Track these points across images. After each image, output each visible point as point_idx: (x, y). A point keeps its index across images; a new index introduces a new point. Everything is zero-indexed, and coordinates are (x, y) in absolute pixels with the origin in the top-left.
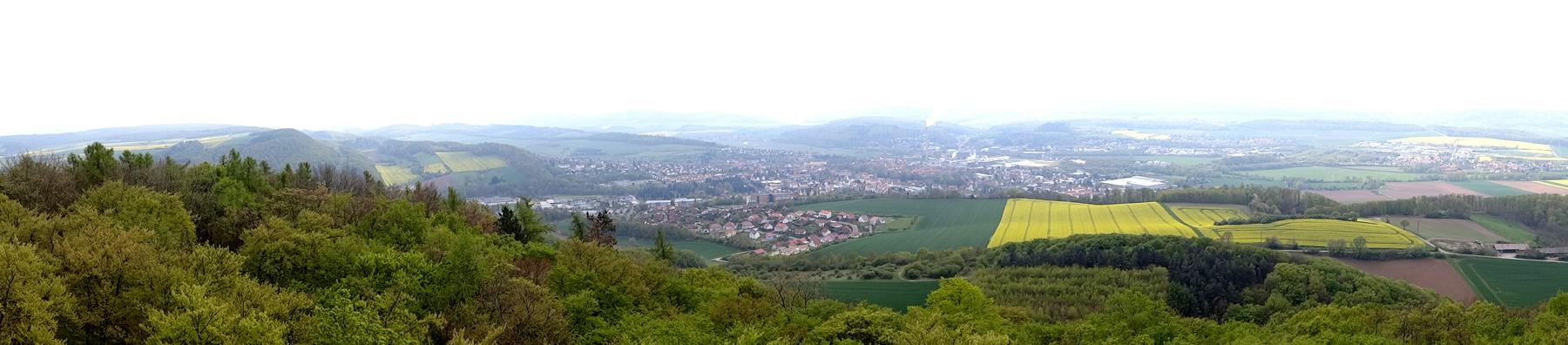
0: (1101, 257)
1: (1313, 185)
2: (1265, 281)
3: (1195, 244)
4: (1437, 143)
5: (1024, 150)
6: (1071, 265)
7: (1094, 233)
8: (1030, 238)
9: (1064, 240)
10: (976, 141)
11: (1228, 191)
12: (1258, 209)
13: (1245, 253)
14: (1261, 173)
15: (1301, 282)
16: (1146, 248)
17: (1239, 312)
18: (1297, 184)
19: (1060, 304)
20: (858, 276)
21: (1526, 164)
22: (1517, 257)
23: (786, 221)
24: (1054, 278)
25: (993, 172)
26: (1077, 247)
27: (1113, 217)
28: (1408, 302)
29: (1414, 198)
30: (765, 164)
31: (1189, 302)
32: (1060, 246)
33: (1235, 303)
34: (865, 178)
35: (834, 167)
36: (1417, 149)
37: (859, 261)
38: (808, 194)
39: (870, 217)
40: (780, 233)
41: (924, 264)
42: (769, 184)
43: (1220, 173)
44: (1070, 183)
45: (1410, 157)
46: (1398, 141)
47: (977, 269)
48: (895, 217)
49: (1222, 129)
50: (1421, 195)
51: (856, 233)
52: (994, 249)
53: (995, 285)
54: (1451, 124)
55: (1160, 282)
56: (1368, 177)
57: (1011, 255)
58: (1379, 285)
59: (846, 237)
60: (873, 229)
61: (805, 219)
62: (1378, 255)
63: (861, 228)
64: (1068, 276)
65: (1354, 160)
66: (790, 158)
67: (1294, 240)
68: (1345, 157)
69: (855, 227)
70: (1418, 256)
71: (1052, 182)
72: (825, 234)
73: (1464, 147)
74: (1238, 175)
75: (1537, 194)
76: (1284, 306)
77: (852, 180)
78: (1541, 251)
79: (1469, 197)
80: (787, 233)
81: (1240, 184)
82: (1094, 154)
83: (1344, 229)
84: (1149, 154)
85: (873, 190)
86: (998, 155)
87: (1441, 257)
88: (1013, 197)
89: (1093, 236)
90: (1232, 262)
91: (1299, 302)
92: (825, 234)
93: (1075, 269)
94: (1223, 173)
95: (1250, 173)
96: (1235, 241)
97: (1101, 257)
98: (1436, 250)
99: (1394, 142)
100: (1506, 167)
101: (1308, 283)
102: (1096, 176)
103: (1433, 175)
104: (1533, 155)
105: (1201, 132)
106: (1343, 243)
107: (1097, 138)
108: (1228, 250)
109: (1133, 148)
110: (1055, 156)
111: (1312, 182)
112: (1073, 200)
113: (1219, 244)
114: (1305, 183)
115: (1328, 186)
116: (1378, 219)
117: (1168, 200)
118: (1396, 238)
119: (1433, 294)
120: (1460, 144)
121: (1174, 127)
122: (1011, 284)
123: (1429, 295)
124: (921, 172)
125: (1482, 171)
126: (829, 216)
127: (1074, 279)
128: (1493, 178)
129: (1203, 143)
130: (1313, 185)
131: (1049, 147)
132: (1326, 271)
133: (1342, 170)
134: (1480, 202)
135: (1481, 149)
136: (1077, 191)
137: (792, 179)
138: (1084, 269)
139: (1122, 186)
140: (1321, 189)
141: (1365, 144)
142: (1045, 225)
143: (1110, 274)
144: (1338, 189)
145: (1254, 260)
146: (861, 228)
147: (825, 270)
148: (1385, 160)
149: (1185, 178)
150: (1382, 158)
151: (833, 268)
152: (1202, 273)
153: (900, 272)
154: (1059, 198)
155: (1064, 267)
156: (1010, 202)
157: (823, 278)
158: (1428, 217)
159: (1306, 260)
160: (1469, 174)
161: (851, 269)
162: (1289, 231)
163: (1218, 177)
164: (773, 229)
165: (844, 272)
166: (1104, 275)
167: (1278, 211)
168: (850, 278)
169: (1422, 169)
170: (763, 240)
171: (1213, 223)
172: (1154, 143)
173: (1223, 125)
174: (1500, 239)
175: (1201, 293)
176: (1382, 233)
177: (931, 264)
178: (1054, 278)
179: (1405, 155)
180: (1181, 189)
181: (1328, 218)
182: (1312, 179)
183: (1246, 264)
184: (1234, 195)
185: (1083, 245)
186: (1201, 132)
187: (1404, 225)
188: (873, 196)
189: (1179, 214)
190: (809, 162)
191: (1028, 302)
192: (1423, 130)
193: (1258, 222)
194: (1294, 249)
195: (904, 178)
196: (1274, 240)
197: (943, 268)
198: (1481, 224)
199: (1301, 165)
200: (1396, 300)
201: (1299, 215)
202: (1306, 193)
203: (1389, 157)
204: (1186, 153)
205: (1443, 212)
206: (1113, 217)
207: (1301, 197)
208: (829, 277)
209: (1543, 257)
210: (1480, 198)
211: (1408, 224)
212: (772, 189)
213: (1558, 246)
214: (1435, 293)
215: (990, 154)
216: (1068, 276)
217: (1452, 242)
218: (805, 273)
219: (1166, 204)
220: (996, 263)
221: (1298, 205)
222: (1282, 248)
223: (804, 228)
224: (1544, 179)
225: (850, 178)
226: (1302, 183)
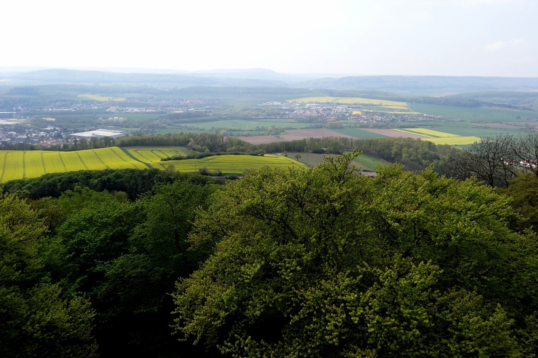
1: (233, 133)
3: (147, 173)
7: (65, 172)
9: (37, 179)
11: (171, 137)
12: (194, 149)
14: (195, 125)
21: (388, 117)
26: (49, 183)
27: (81, 160)
32: (34, 184)
43: (166, 125)
44: (43, 137)
45: (302, 112)
46: (294, 100)
54: (333, 88)
56: (272, 127)
65: (262, 115)
67: (219, 170)
71: (25, 137)
73: (342, 104)
74: (179, 126)
83: (255, 162)
84: (110, 113)
89: (63, 174)
94: (168, 125)
95: (188, 125)
96: (176, 171)
99: (290, 101)
100: (372, 119)
102: (65, 130)
103: (318, 124)
105: (150, 95)
107: (65, 101)
109: (96, 108)
110: (25, 115)
111: (233, 130)
112: (45, 149)
113: (164, 173)
114: (227, 131)
115: (244, 133)
116: (279, 154)
121: (128, 92)
125: (354, 121)
131: (20, 108)
133: (254, 123)
135: (354, 106)
136: (49, 143)
139: (88, 137)
144: (251, 136)
148: (284, 114)
154: (32, 148)
158: (314, 152)
160: (345, 123)
162: (215, 164)
163: (165, 128)
167: (208, 150)
169: (311, 120)
172: (114, 104)
174: (365, 168)
179: (298, 112)
181: (243, 154)
182: (233, 128)
184: (175, 140)
185: (54, 181)
186: (150, 95)
187: (297, 158)
192: (311, 92)
193: (193, 158)
199: (224, 119)
201: (223, 152)
203: (287, 112)
204: (139, 111)
205: (325, 149)
206: (81, 160)
207: (224, 140)
210: (352, 139)
211: (300, 157)
219: (124, 148)
221: (222, 146)
222: (211, 175)
224: (401, 127)
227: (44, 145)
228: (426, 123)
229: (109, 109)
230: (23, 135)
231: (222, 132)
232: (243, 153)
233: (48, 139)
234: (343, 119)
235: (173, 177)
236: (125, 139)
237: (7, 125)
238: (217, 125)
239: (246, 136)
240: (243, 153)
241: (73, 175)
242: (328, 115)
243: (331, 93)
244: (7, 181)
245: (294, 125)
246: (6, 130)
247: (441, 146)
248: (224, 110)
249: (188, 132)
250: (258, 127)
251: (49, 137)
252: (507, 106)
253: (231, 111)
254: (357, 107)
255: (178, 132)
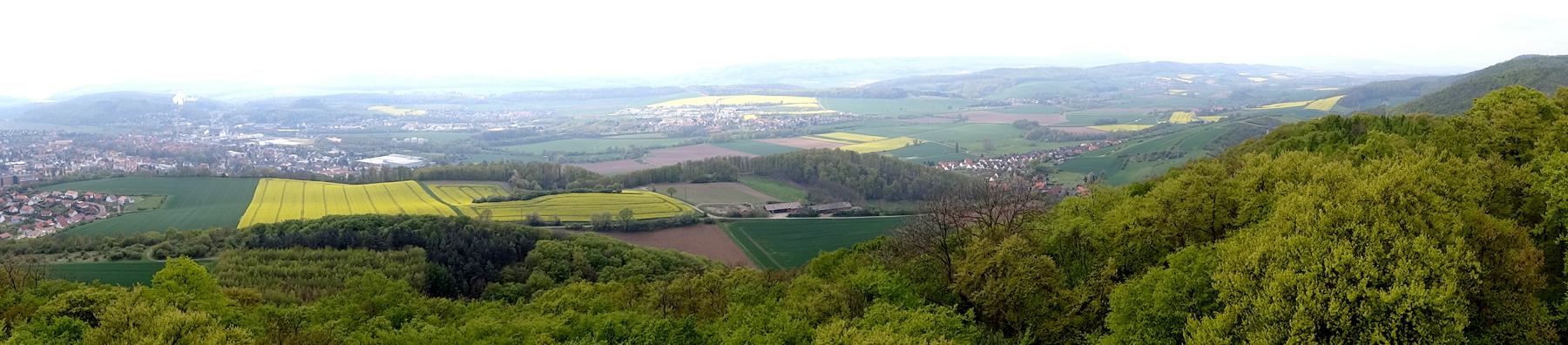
0: (355, 239)
1: (575, 158)
2: (526, 259)
3: (453, 223)
4: (698, 104)
5: (279, 127)
6: (324, 248)
8: (281, 220)
9: (316, 221)
10: (229, 116)
12: (519, 186)
13: (506, 231)
15: (564, 258)
16: (402, 228)
17: (498, 291)
18: (558, 158)
19: (312, 287)
20: (105, 257)
21: (793, 119)
22: (789, 216)
23: (31, 203)
24: (306, 260)
25: (246, 150)
27: (369, 198)
28: (680, 271)
29: (679, 163)
30: (8, 145)
31: (448, 282)
32: (313, 228)
33: (494, 282)
34: (113, 156)
35: (81, 145)
36: (679, 112)
37: (106, 242)
38: (54, 175)
39: (118, 196)
40: (25, 216)
41: (173, 244)
42: (13, 166)
44: (325, 162)
45: (673, 121)
46: (660, 104)
47: (225, 250)
48: (145, 196)
49: (481, 102)
50: (686, 159)
51: (103, 213)
52: (243, 230)
53: (241, 267)
55: (417, 263)
57: (261, 237)
58: (650, 256)
59: (92, 217)
60: (122, 209)
61: (51, 200)
62: (646, 225)
63: (109, 208)
64: (321, 258)
65: (615, 130)
66: (34, 138)
68: (605, 127)
69: (102, 207)
70: (688, 223)
71: (306, 162)
72: (72, 215)
73: (727, 106)
74: (498, 150)
75: (805, 150)
76: (547, 284)
77: (100, 159)
78: (814, 208)
79: (735, 158)
80: (33, 216)
81: (500, 160)
82: (350, 132)
83: (608, 202)
84: (406, 131)
85: (121, 168)
86: (253, 132)
87: (710, 222)
88: (266, 177)
89: (347, 217)
90: (491, 240)
91: (563, 280)
92: (72, 215)
93: (327, 251)
95: (511, 148)
96: (494, 219)
97: (355, 239)
98: (705, 216)
100: (772, 124)
101: (572, 260)
102: (352, 155)
103: (696, 138)
104: (799, 109)
105: (459, 106)
106: (609, 216)
107: (353, 115)
108: (485, 229)
110: (309, 134)
111: (574, 155)
113: (478, 223)
115: (591, 158)
116: (644, 188)
117: (425, 178)
118: (664, 206)
119: (705, 261)
120: (722, 103)
121: (431, 102)
122: (259, 266)
123: (702, 262)
124: (171, 149)
125: (747, 130)
126: (75, 195)
127: (326, 262)
128: (757, 137)
129: (461, 118)
130: (575, 158)
131: (304, 124)
132: (590, 247)
134: (747, 163)
135: (744, 108)
136: (332, 170)
137: (37, 160)
138: (336, 252)
139: (379, 165)
140: (583, 162)
141: (626, 112)
142: (299, 206)
143: (364, 255)
144: (601, 161)
145: (514, 238)
146: (109, 208)
147: (71, 251)
149: (444, 155)
150: (643, 124)
151: (79, 250)
152: (461, 252)
153: (149, 252)
154: (314, 178)
155: (316, 249)
156: (262, 181)
157: (70, 260)
158: (696, 182)
159: (569, 237)
161: (97, 250)
163: (478, 153)
164: (19, 212)
165: (90, 254)
166: (359, 257)
167: (539, 187)
168: (96, 260)
169: (686, 132)
170: (9, 224)
171: (472, 200)
172: (412, 119)
173: (482, 98)
175: (460, 272)
176: (649, 203)
177: (180, 244)
178: (306, 260)
180: (439, 166)
182: (573, 151)
183: (505, 242)
186: (459, 106)
187: (671, 192)
188: (121, 175)
189: (437, 193)
190: (54, 141)
191: (278, 285)
192: (683, 91)
194: (556, 225)
195: (154, 156)
196: (535, 217)
197: (192, 248)
198: (750, 186)
199: (561, 138)
200: (668, 269)
201: (561, 190)
202: (567, 167)
203: (650, 123)
205: (710, 176)
207: (562, 171)
208: (75, 259)
209: (817, 214)
210: (747, 158)
212: (16, 170)
213: (831, 202)
214: (707, 259)
215: (246, 131)
216: (321, 258)
217: (721, 207)
218: (52, 255)
219: (423, 182)
220: (243, 244)
221: (558, 180)
222: (543, 225)
223: (51, 210)
224: (813, 133)
225: (97, 156)
226: (562, 156)
227: (326, 174)
228: (843, 125)
229: (406, 126)
230: (305, 159)
231: (558, 157)
232: (590, 189)
233: (331, 166)
234: (731, 128)
235: (489, 230)
236: (425, 171)
237: (289, 146)
238: (550, 147)
239: (593, 162)
240: (590, 189)
241: (358, 220)
242: (710, 123)
243: (712, 92)
244: (284, 220)
245: (663, 143)
246: (287, 153)
247: (866, 156)
248: (559, 124)
249: (510, 158)
250: (610, 148)
251: (333, 164)
252: (932, 94)
253: (569, 125)
254: (750, 109)
255: (497, 159)
